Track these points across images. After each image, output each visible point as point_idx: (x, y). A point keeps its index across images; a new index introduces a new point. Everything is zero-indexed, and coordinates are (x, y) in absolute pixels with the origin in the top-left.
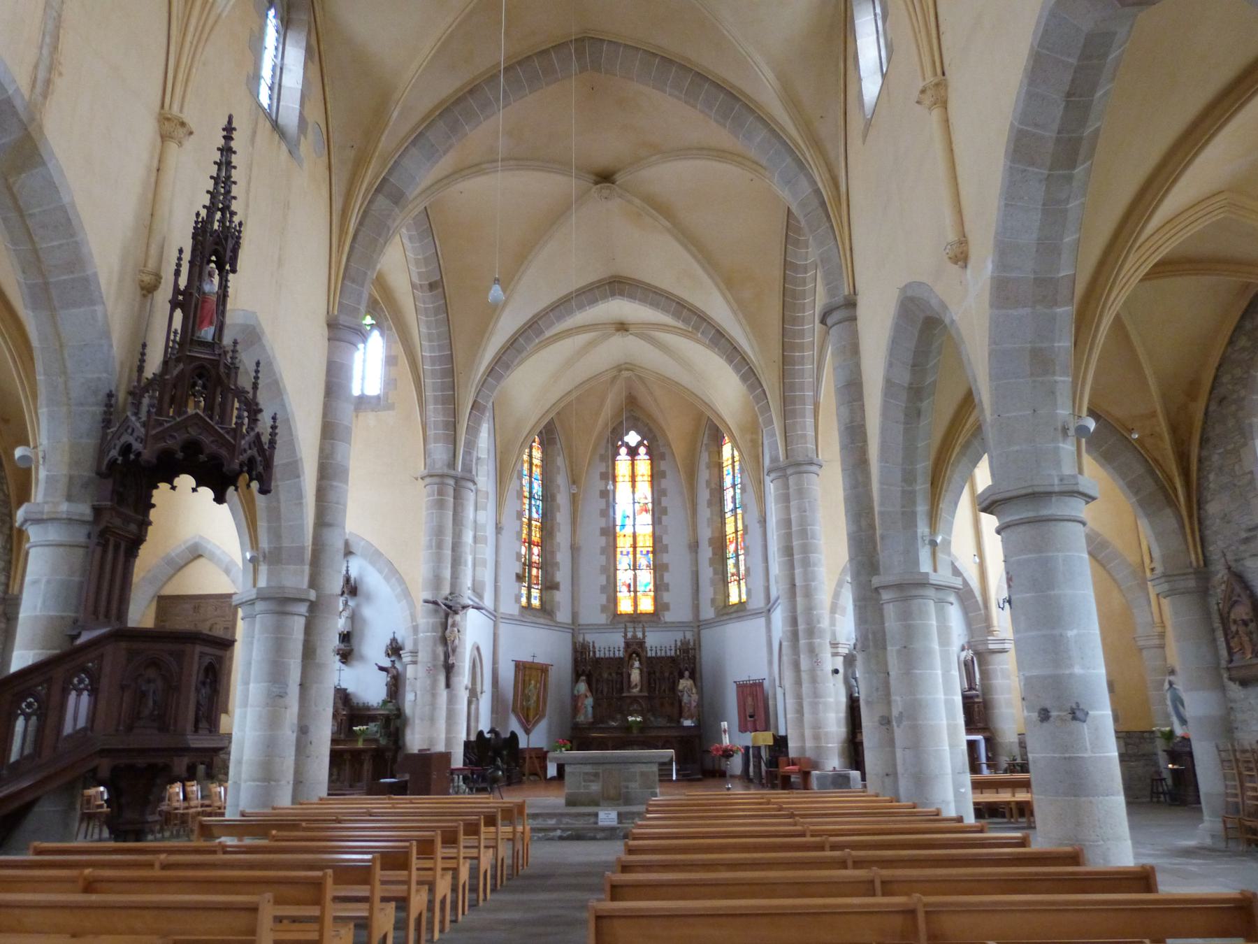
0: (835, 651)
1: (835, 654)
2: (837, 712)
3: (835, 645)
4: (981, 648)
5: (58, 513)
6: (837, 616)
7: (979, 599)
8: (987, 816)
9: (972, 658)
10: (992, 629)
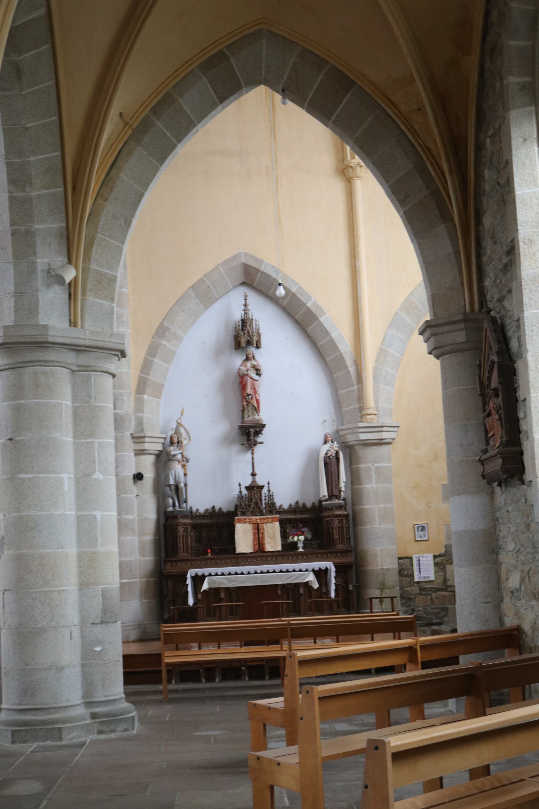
0: (140, 447)
1: (139, 453)
2: (142, 533)
3: (138, 439)
4: (350, 439)
5: (84, 293)
6: (145, 397)
7: (352, 369)
8: (203, 680)
9: (337, 453)
10: (365, 412)
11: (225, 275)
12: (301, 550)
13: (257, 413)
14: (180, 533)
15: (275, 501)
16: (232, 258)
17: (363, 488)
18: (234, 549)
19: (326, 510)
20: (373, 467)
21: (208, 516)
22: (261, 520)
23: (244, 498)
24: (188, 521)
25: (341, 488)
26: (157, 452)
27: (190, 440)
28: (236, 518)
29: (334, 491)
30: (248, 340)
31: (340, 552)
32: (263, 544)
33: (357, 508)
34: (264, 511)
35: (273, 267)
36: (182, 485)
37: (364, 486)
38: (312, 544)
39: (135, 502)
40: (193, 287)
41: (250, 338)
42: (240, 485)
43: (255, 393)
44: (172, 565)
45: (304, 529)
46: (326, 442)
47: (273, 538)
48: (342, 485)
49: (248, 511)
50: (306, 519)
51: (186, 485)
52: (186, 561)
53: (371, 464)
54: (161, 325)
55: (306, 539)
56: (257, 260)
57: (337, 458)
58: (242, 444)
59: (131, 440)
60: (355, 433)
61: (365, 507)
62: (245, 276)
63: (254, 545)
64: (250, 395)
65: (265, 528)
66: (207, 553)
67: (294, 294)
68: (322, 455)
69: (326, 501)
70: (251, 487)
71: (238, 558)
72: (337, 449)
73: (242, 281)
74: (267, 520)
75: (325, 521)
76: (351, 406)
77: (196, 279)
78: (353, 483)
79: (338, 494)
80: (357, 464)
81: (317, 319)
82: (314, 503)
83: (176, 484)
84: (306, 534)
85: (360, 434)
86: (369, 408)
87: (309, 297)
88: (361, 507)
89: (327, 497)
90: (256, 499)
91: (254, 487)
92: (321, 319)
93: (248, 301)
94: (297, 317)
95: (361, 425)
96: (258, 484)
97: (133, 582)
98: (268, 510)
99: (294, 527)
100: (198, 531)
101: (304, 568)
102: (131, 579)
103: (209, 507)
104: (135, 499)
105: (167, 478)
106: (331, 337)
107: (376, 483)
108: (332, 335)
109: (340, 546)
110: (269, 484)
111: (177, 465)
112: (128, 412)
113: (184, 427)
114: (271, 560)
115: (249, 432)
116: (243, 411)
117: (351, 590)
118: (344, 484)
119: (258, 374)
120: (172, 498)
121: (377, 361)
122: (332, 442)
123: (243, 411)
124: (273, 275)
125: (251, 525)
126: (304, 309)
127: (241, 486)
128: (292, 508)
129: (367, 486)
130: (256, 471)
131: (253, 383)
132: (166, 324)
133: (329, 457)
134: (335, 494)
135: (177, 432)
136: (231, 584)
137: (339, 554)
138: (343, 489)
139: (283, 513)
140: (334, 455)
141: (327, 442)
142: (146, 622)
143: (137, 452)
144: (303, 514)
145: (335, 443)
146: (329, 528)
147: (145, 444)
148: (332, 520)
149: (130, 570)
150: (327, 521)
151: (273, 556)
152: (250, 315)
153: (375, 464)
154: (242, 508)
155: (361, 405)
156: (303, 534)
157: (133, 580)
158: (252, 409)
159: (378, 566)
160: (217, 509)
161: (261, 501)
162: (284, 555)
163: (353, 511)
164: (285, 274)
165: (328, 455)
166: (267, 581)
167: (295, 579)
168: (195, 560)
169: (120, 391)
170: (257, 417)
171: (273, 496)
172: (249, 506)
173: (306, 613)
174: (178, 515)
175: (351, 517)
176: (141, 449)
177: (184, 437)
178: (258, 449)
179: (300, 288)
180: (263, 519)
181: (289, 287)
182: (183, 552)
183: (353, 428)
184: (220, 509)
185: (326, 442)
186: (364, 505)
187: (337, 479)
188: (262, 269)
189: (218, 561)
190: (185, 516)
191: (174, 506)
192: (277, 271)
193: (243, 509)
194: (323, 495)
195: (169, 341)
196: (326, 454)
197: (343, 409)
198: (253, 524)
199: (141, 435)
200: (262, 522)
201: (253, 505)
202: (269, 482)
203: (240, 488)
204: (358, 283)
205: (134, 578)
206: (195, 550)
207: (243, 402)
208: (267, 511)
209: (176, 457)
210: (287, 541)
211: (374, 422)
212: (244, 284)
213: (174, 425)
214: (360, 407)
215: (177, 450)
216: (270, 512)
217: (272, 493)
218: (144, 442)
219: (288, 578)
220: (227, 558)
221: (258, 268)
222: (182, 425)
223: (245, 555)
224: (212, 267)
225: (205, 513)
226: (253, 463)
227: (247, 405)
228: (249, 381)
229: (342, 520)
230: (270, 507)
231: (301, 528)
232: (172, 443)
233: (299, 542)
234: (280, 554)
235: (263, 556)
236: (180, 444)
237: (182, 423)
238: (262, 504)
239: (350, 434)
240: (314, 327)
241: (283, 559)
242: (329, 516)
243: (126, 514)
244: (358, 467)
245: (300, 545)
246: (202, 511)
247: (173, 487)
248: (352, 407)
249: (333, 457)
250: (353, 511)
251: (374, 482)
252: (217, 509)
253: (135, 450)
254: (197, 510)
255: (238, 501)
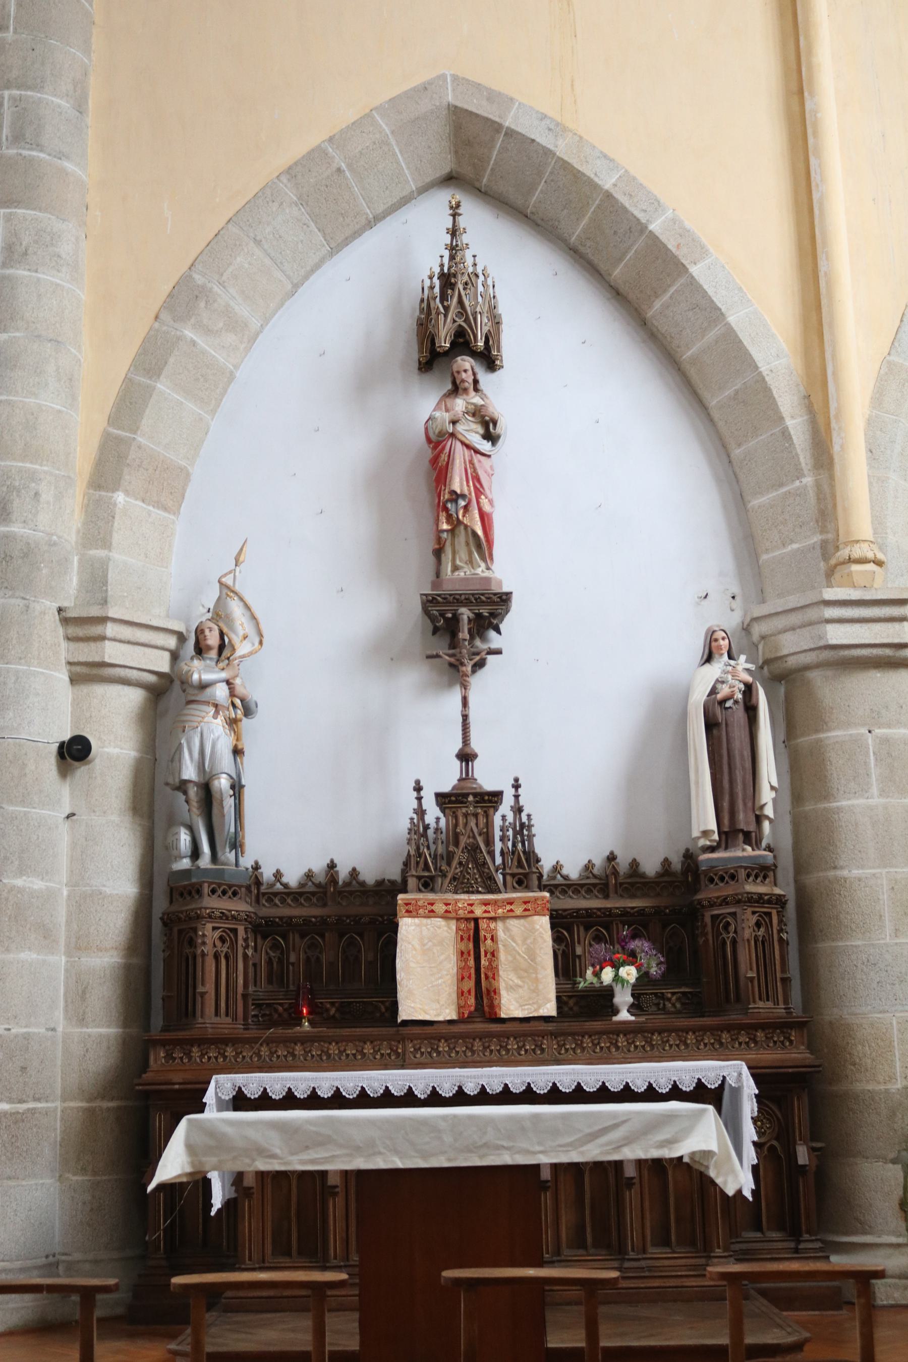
0: (87, 653)
6: (120, 498)
9: (749, 690)
10: (844, 553)
11: (393, 141)
12: (624, 1015)
13: (483, 559)
14: (204, 943)
15: (539, 849)
16: (414, 89)
17: (839, 810)
18: (394, 1007)
19: (711, 880)
20: (870, 739)
21: (313, 894)
22: (489, 908)
23: (430, 832)
24: (240, 906)
25: (762, 807)
26: (152, 679)
27: (261, 643)
28: (400, 896)
29: (741, 816)
30: (460, 326)
31: (763, 1027)
32: (493, 993)
33: (810, 879)
34: (500, 878)
35: (544, 117)
36: (223, 783)
37: (844, 803)
38: (662, 997)
39: (63, 836)
40: (291, 172)
41: (467, 320)
42: (418, 788)
43: (479, 492)
44: (169, 1056)
45: (635, 944)
46: (709, 658)
47: (528, 971)
48: (767, 796)
49: (444, 876)
50: (641, 912)
51: (237, 788)
52: (221, 1042)
53: (864, 731)
54: (185, 281)
55: (644, 978)
56: (492, 96)
57: (751, 710)
58: (429, 657)
59: (61, 631)
60: (811, 624)
61: (845, 873)
62: (456, 152)
63: (461, 993)
64: (463, 496)
65: (501, 934)
66: (297, 1020)
67: (609, 196)
68: (699, 696)
69: (712, 849)
70: (456, 795)
71: (402, 1039)
72: (750, 679)
73: (445, 169)
74: (508, 907)
75: (708, 919)
76: (792, 542)
77: (298, 149)
78: (797, 797)
79: (752, 827)
80: (817, 731)
81: (682, 269)
82: (666, 862)
83: (202, 781)
84: (643, 959)
85: (830, 628)
86: (857, 542)
87: (657, 205)
88: (831, 874)
89: (716, 837)
90: (474, 837)
91: (466, 795)
92: (694, 270)
93: (462, 222)
94: (617, 273)
95: (830, 594)
96: (481, 787)
97: (33, 1111)
98: (513, 875)
99: (598, 939)
100: (275, 946)
101: (663, 1081)
102: (21, 1101)
103: (318, 865)
104: (64, 828)
105: (175, 757)
106: (728, 325)
107: (883, 793)
108: (732, 319)
109: (762, 1008)
110: (516, 786)
111: (209, 718)
112: (55, 538)
113: (241, 599)
114: (519, 1048)
115: (456, 618)
116: (438, 553)
117: (804, 1166)
118: (773, 794)
119: (491, 437)
120: (191, 829)
121: (878, 399)
122: (730, 657)
123: (438, 553)
124: (544, 139)
125: (453, 925)
126: (640, 243)
127: (422, 793)
128: (595, 876)
129: (849, 803)
130: (476, 745)
131: (471, 462)
132: (198, 279)
133: (722, 702)
134: (742, 826)
135: (219, 614)
136: (305, 1156)
137: (760, 1035)
138: (769, 811)
139: (564, 892)
140: (739, 696)
141: (716, 656)
142: (77, 1256)
143: (78, 669)
144: (633, 896)
145: (743, 658)
146: (724, 943)
147: (107, 642)
148: (734, 914)
149: (24, 1069)
150: (714, 918)
151: (525, 1035)
152: (469, 261)
153: (877, 731)
154: (422, 865)
155: (830, 536)
156: (632, 958)
157: (31, 1105)
158: (467, 544)
159: (892, 1078)
160: (343, 873)
161: (489, 842)
162: (565, 1034)
163: (801, 891)
164: (581, 137)
165: (719, 696)
166: (486, 1145)
167: (628, 1141)
168: (251, 1041)
169: (28, 465)
170: (481, 570)
171: (530, 827)
172: (449, 857)
173: (644, 1251)
174: (201, 885)
175: (791, 906)
176: (90, 659)
177: (241, 633)
178: (479, 683)
179: (628, 178)
180: (496, 902)
181: (592, 176)
182: (217, 1013)
183: (802, 607)
184: (354, 873)
185: (709, 658)
186: (842, 868)
187: (749, 777)
188: (508, 123)
189: (333, 1049)
190: (230, 891)
191: (196, 853)
192: (558, 128)
193: (426, 867)
194: (702, 828)
195: (208, 331)
196: (713, 691)
197: (764, 557)
198: (458, 919)
199: (95, 612)
200: (492, 914)
201: (460, 855)
202: (516, 780)
203: (419, 799)
204: (813, 161)
205: (38, 1100)
206: (258, 1006)
207: (437, 521)
208: (508, 878)
209: (209, 691)
210: (575, 983)
211: (875, 586)
212: (450, 180)
213: (210, 598)
214: (824, 544)
215: (217, 669)
216: (520, 882)
217: (529, 816)
218: (103, 638)
219: (593, 1136)
220: (364, 1040)
221: (497, 119)
222: (236, 593)
223: (428, 1030)
224: (352, 115)
225: (302, 885)
226: (465, 717)
227: (452, 531)
228: (460, 455)
229: (769, 914)
230: (520, 865)
231: (623, 943)
232: (200, 650)
233: (617, 989)
234: (551, 1027)
235: (490, 1035)
236: (226, 653)
237: (237, 588)
238: (492, 854)
239: (793, 629)
240: (671, 297)
241: (560, 1046)
242: (725, 902)
243: (21, 872)
244: (820, 740)
245: (623, 998)
246: (292, 878)
247: (193, 791)
248: (795, 546)
249: (736, 702)
250: (801, 891)
251: (875, 790)
252: (343, 873)
253: (70, 663)
254: (278, 875)
255: (409, 841)
